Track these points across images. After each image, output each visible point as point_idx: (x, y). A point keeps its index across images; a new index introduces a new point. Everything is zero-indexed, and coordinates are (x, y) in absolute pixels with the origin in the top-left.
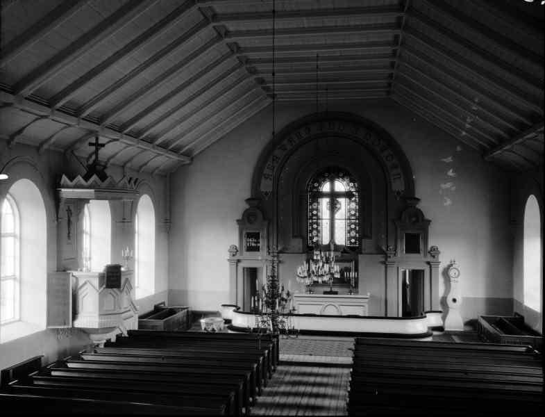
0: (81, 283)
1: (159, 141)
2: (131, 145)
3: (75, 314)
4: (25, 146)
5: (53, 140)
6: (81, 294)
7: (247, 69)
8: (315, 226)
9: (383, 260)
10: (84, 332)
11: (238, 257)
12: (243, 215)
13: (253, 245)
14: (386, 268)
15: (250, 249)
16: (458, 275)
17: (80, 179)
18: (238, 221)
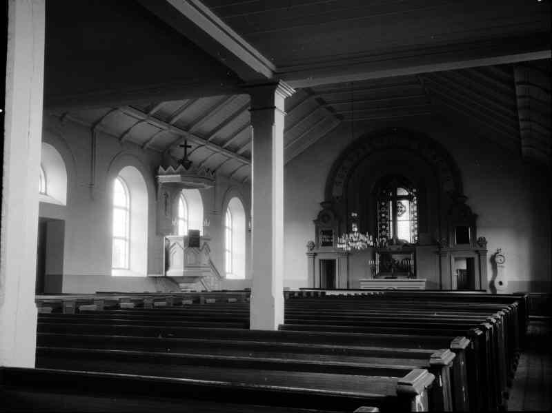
0: (171, 244)
1: (240, 152)
2: (216, 152)
3: (167, 267)
4: (132, 144)
5: (151, 142)
6: (172, 251)
7: (317, 99)
8: (384, 227)
9: (438, 250)
10: (173, 280)
11: (315, 251)
12: (319, 216)
13: (327, 240)
14: (440, 257)
15: (325, 244)
16: (504, 261)
17: (171, 168)
18: (314, 221)
